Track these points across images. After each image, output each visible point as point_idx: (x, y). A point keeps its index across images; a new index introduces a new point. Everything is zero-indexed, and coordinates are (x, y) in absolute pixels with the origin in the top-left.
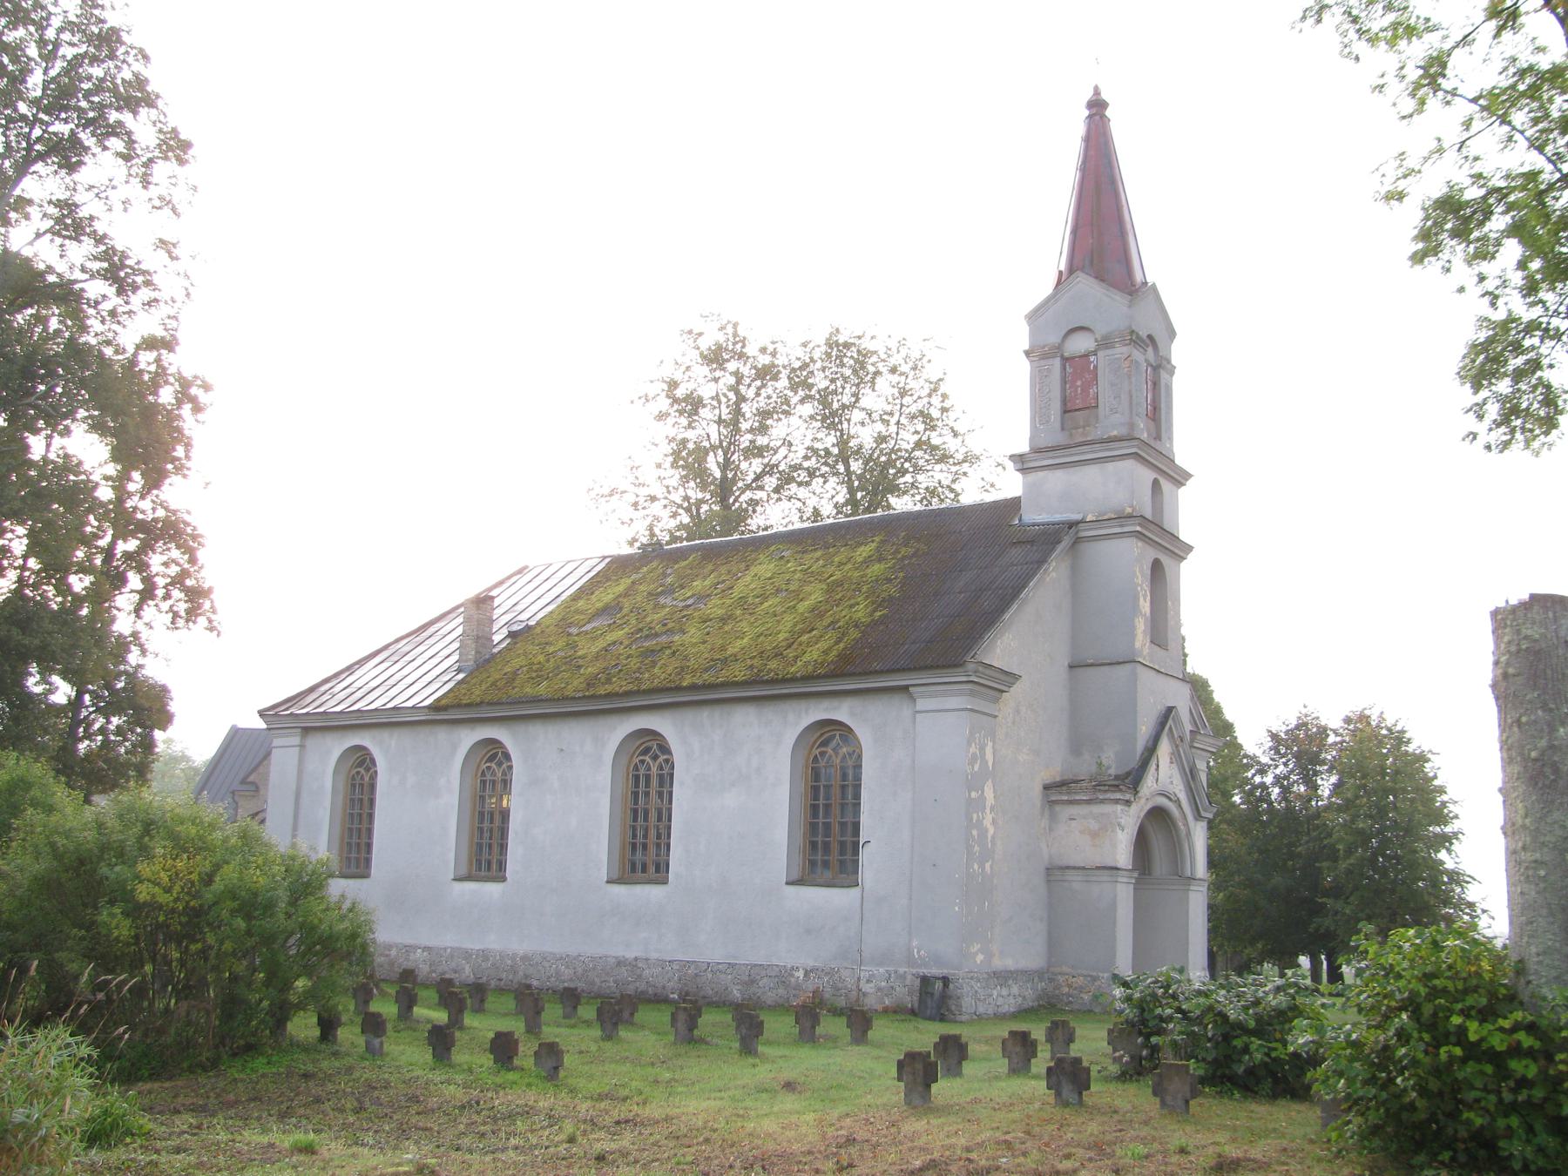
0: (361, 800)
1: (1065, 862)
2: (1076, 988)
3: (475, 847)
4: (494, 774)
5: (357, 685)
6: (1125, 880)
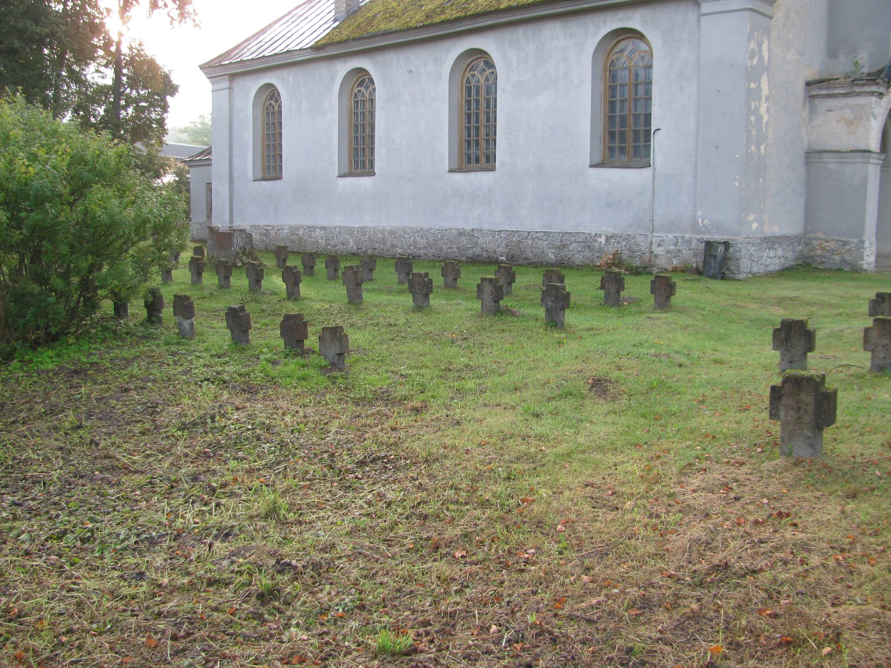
0: (274, 123)
1: (822, 147)
2: (828, 251)
3: (353, 151)
4: (363, 94)
5: (266, 40)
6: (875, 161)
